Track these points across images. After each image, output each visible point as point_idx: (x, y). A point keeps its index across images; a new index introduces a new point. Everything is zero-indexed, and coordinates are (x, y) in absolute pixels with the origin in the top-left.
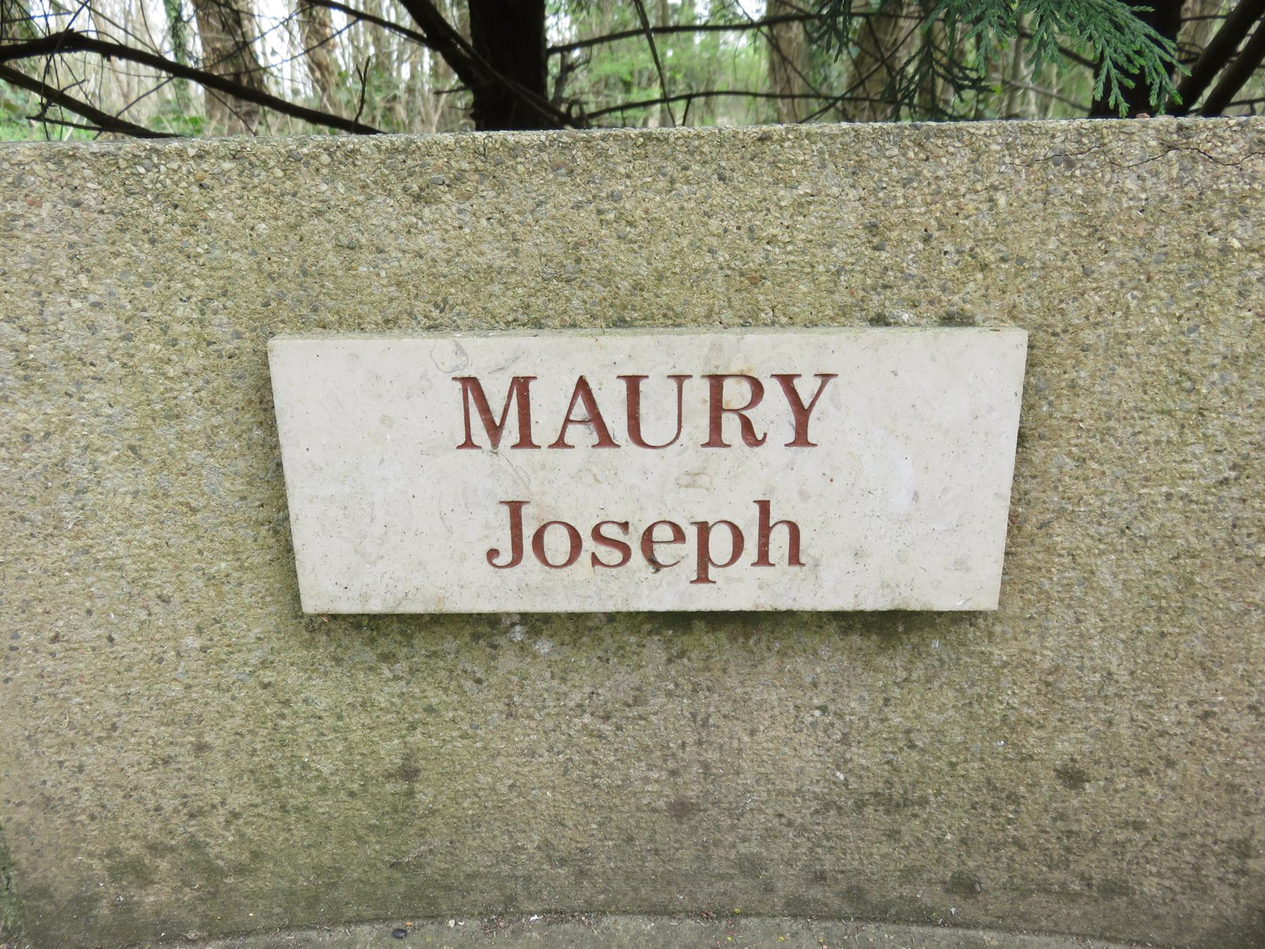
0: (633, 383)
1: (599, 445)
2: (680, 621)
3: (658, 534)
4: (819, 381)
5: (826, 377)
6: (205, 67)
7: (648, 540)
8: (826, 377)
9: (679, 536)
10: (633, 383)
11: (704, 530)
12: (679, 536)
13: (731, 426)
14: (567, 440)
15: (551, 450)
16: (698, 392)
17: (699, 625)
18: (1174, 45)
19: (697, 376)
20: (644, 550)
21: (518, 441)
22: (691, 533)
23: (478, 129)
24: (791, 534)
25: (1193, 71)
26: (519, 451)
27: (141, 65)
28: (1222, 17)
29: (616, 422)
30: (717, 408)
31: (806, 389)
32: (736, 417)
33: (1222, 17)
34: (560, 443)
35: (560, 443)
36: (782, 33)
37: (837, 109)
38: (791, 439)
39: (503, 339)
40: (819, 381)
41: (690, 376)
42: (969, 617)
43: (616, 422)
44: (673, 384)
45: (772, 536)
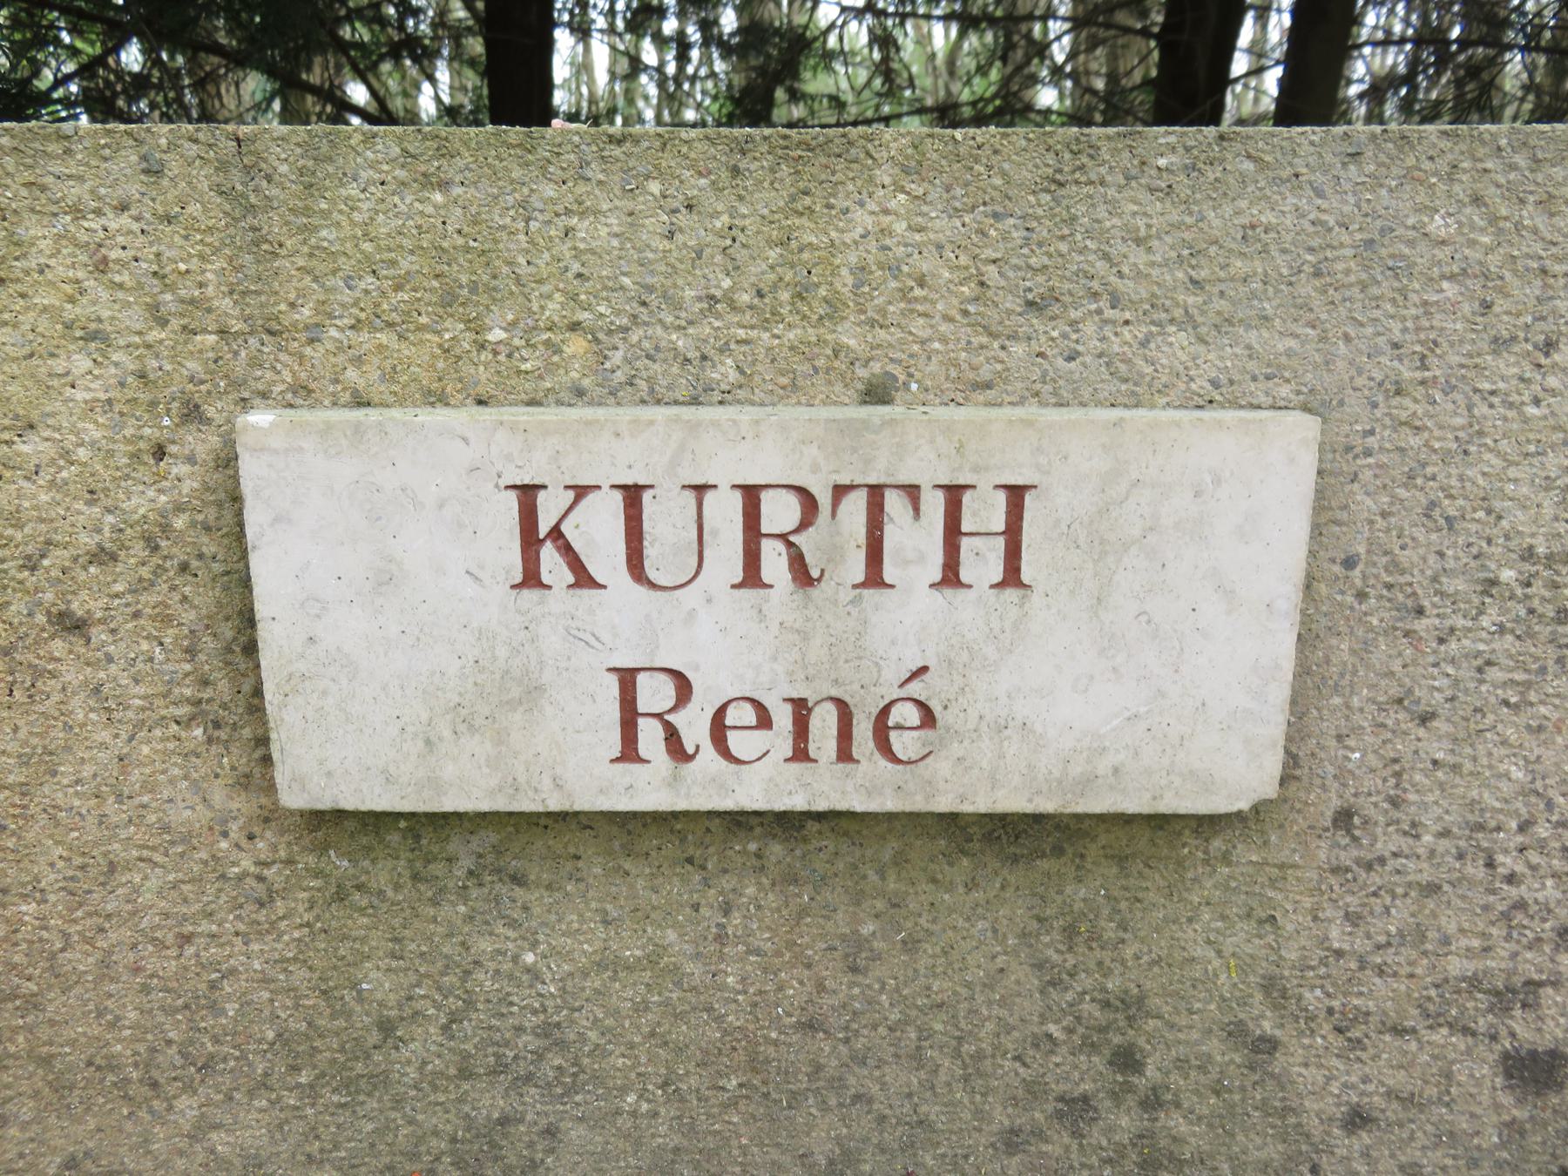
2: (787, 824)
3: (897, 715)
4: (571, 494)
9: (764, 720)
11: (801, 710)
12: (764, 720)
13: (774, 561)
15: (571, 591)
16: (725, 511)
17: (813, 827)
21: (740, 579)
22: (783, 718)
32: (780, 546)
37: (601, 31)
40: (571, 494)
41: (544, 487)
44: (690, 496)
45: (815, 723)
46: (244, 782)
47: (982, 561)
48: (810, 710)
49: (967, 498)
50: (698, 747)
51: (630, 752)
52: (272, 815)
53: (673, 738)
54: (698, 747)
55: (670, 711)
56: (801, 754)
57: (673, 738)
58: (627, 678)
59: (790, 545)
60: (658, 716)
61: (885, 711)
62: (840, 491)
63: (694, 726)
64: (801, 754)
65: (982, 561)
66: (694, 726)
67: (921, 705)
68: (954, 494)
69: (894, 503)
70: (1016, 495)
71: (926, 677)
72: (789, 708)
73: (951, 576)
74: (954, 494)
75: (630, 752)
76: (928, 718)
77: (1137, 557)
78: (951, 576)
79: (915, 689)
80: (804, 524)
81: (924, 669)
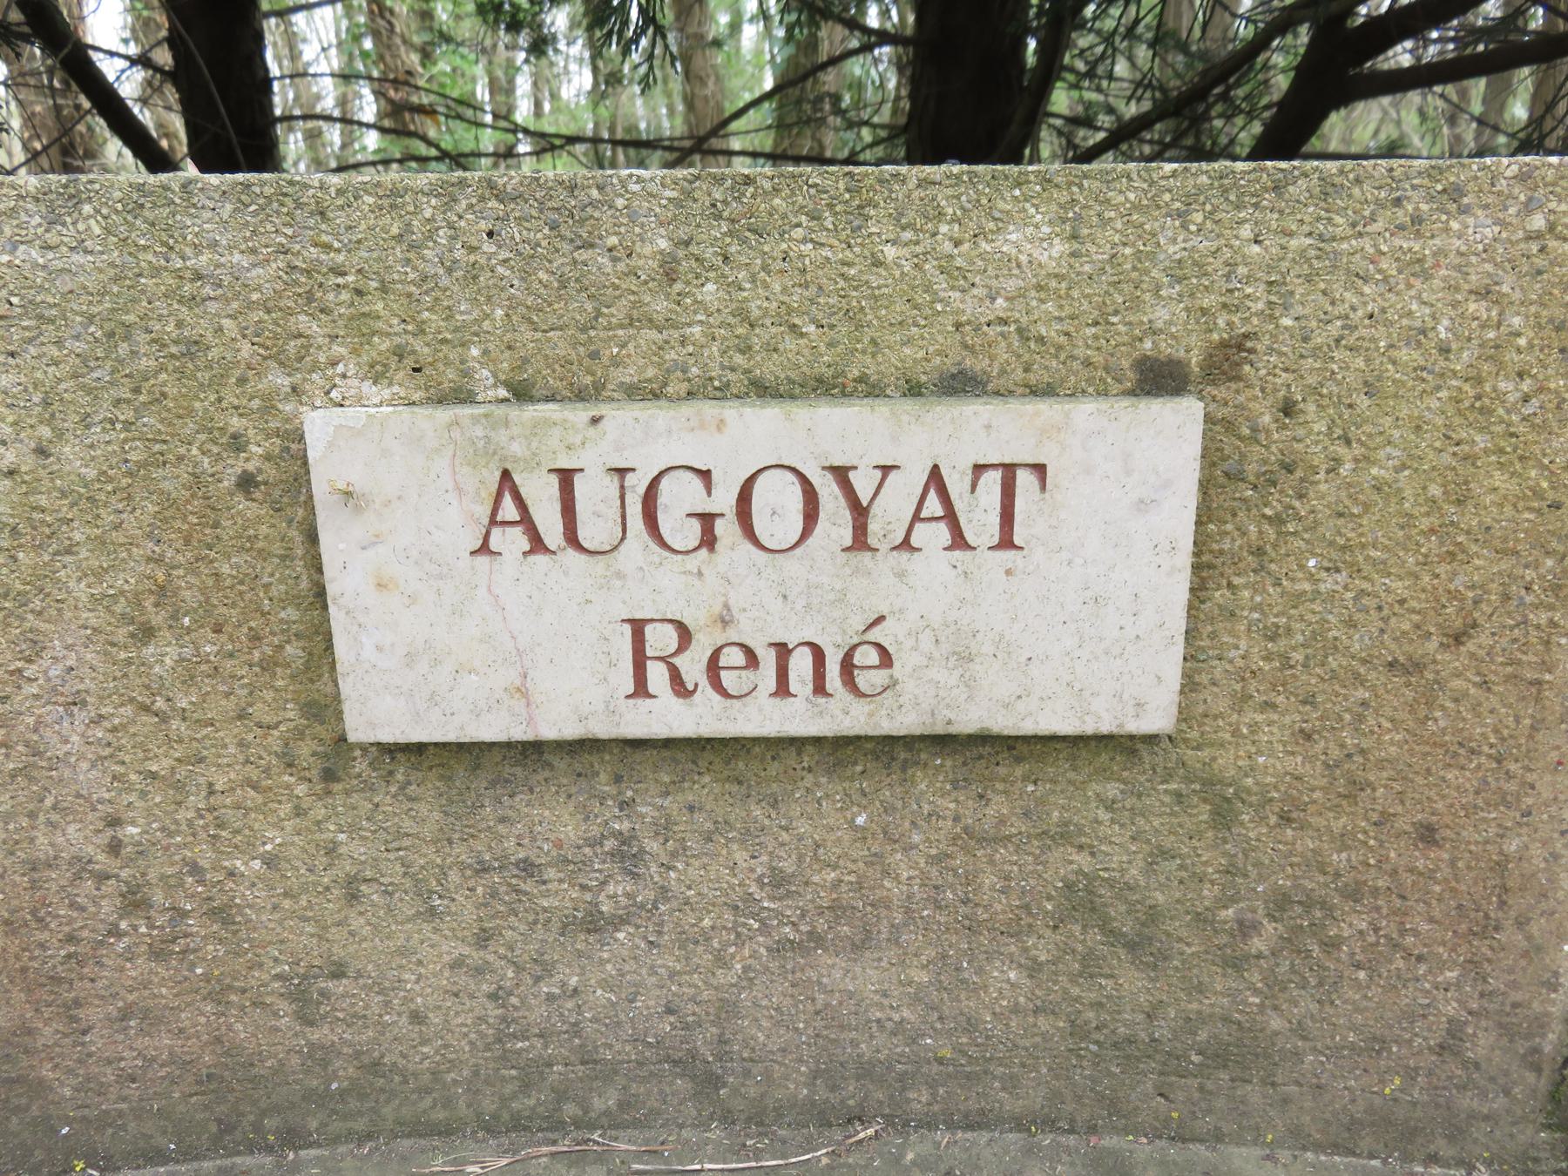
0: (566, 478)
1: (531, 552)
3: (858, 659)
5: (886, 470)
7: (848, 666)
8: (886, 470)
10: (566, 478)
11: (783, 651)
14: (914, 541)
18: (175, 143)
21: (696, 543)
22: (768, 659)
23: (911, 160)
26: (532, 558)
29: (550, 525)
31: (863, 485)
34: (906, 545)
35: (906, 545)
36: (697, 91)
40: (879, 474)
42: (1151, 739)
43: (550, 525)
44: (879, 474)
48: (790, 651)
50: (696, 685)
51: (641, 689)
52: (337, 758)
53: (676, 678)
54: (696, 685)
55: (672, 655)
56: (783, 689)
57: (676, 678)
58: (638, 628)
59: (668, 663)
62: (979, 469)
63: (693, 667)
64: (783, 689)
66: (693, 667)
69: (1024, 479)
71: (884, 624)
72: (773, 652)
75: (641, 689)
76: (886, 659)
77: (1006, 514)
79: (873, 636)
80: (681, 649)
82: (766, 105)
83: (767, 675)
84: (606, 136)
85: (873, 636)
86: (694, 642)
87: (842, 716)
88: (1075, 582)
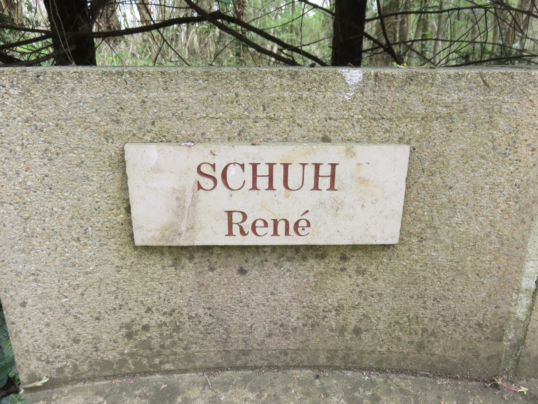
3: (300, 224)
6: (215, 28)
9: (266, 224)
11: (276, 223)
12: (266, 224)
15: (267, 191)
16: (310, 171)
19: (263, 163)
20: (252, 230)
22: (271, 224)
24: (286, 226)
25: (198, 17)
27: (260, 36)
28: (369, 20)
30: (317, 176)
33: (369, 20)
38: (267, 187)
39: (284, 147)
44: (301, 166)
46: (389, 248)
47: (325, 183)
49: (274, 166)
51: (230, 233)
52: (136, 248)
56: (275, 233)
58: (230, 213)
60: (237, 224)
61: (255, 222)
63: (247, 226)
64: (275, 233)
65: (325, 183)
66: (247, 228)
67: (307, 221)
68: (255, 166)
70: (333, 166)
72: (272, 222)
73: (316, 187)
74: (255, 166)
75: (230, 233)
76: (309, 225)
77: (345, 176)
78: (316, 187)
79: (304, 217)
80: (243, 222)
81: (307, 211)
82: (436, 14)
83: (270, 229)
84: (440, 42)
85: (304, 217)
86: (247, 215)
87: (293, 240)
88: (362, 192)
